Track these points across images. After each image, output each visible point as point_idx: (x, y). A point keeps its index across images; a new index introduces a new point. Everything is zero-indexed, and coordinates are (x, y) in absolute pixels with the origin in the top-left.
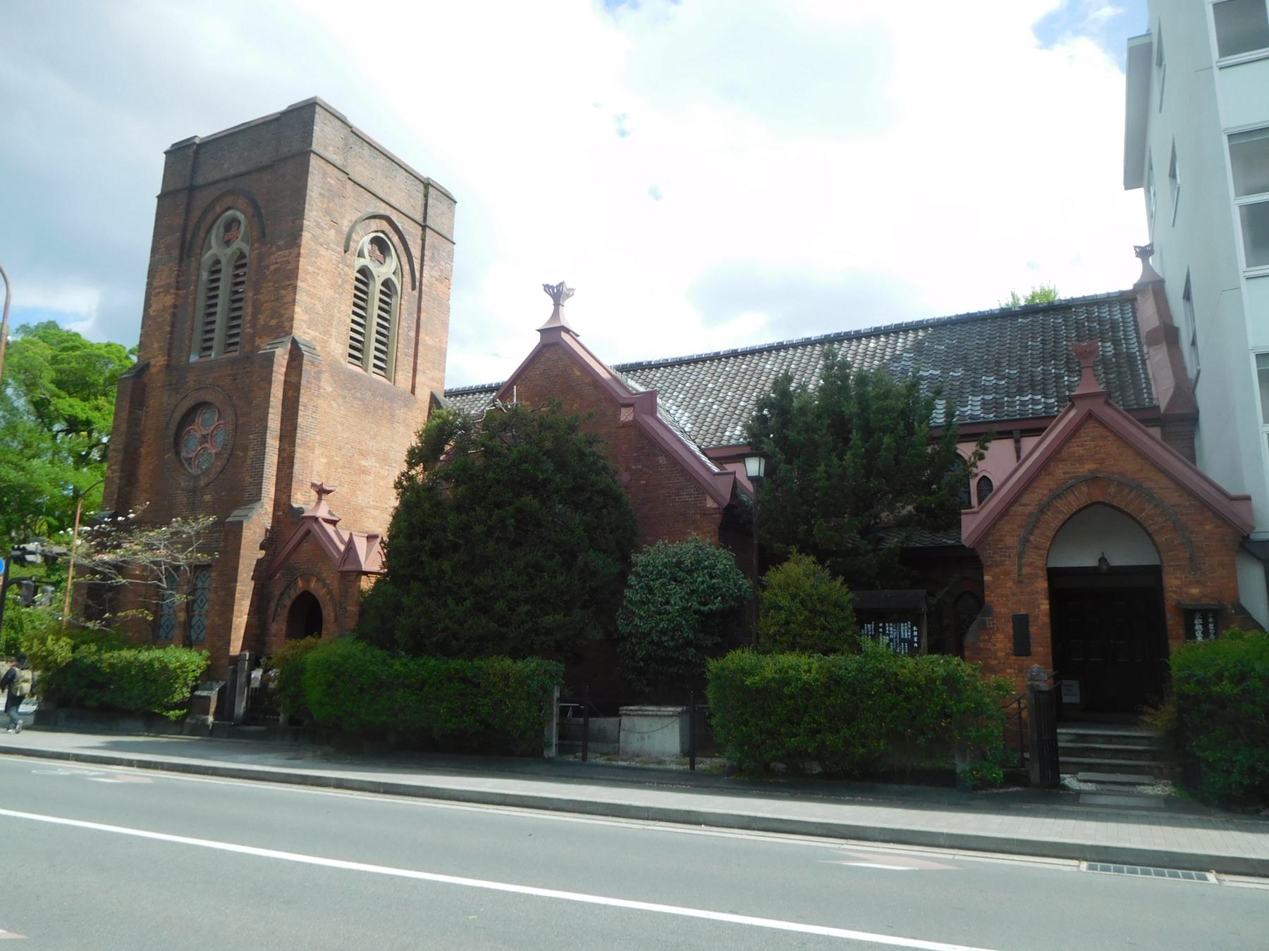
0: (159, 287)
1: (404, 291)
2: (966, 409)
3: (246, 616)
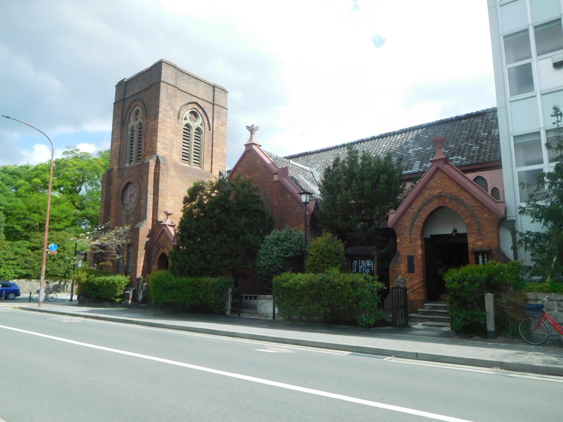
0: (115, 139)
1: (206, 131)
2: (428, 165)
3: (143, 263)
